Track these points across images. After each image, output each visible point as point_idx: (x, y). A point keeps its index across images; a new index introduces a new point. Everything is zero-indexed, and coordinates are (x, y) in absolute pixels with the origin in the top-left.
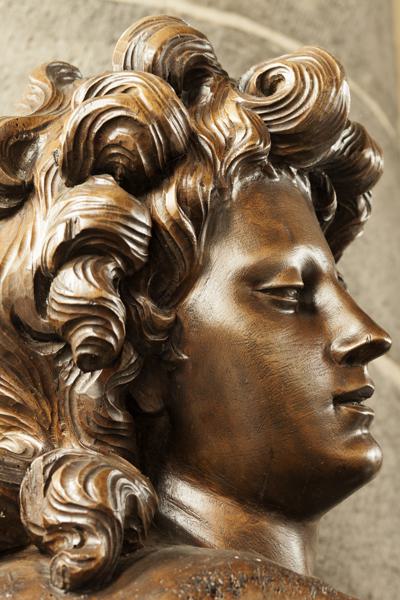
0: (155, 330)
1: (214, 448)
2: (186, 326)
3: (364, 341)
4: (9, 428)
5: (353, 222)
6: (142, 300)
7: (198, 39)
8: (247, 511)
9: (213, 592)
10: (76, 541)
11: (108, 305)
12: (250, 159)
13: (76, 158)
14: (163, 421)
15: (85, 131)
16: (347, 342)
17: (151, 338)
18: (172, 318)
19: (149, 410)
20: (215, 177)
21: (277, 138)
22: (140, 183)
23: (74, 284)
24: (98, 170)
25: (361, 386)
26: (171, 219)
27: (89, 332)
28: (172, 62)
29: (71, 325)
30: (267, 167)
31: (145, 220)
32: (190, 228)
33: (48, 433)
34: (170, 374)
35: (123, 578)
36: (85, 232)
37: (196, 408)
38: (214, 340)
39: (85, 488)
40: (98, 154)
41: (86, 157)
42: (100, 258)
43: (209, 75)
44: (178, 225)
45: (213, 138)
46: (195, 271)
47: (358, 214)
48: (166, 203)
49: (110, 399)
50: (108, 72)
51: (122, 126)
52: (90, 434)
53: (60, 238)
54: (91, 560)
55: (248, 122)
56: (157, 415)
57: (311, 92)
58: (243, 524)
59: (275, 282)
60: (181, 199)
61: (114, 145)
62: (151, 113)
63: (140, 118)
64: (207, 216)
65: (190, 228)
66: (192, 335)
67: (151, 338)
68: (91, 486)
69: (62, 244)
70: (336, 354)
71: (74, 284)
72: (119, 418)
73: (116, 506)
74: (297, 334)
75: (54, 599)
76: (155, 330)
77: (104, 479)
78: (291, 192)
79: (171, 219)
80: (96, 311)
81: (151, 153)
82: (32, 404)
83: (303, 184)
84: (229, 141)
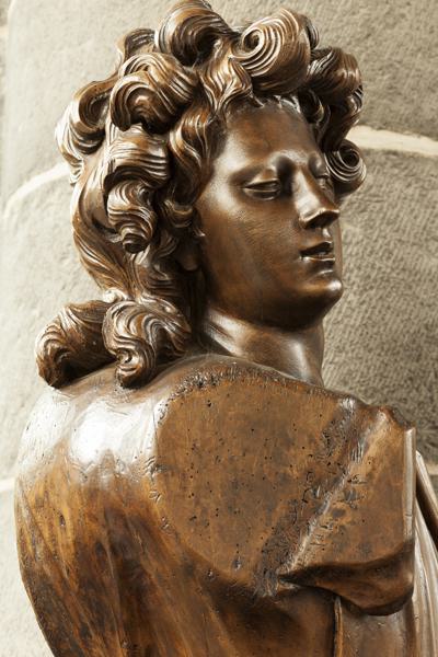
0: (177, 221)
1: (229, 291)
2: (202, 214)
3: (318, 213)
4: (111, 286)
5: (346, 117)
6: (168, 203)
7: (205, 16)
8: (255, 328)
9: (201, 385)
10: (127, 359)
11: (136, 213)
12: (237, 99)
13: (120, 116)
14: (200, 274)
15: (120, 99)
16: (309, 215)
17: (178, 226)
18: (190, 210)
19: (189, 269)
20: (213, 115)
21: (256, 81)
22: (158, 127)
23: (118, 201)
24: (135, 122)
25: (321, 242)
26: (180, 150)
27: (129, 230)
28: (186, 34)
29: (119, 225)
30: (253, 100)
31: (160, 153)
32: (195, 154)
33: (128, 288)
34: (198, 245)
35: (158, 377)
36: (119, 168)
37: (215, 266)
38: (222, 221)
39: (128, 326)
40: (132, 112)
41: (126, 114)
42: (131, 182)
43: (217, 38)
44: (185, 154)
45: (214, 87)
46: (207, 175)
47: (349, 110)
48: (175, 138)
49: (157, 267)
50: (254, 18)
51: (141, 94)
52: (149, 290)
53: (105, 174)
54: (133, 369)
55: (233, 73)
56: (197, 271)
57: (276, 43)
58: (253, 337)
59: (257, 180)
60: (185, 135)
61: (138, 106)
62: (158, 83)
63: (151, 88)
64: (211, 143)
65: (195, 154)
66: (205, 221)
67: (178, 226)
68: (132, 325)
69: (107, 177)
70: (302, 223)
71: (118, 201)
72: (166, 277)
73: (147, 337)
74: (273, 213)
75: (437, 303)
76: (177, 221)
77: (139, 321)
78: (290, 112)
79: (180, 150)
80: (130, 217)
81: (163, 110)
82: (117, 271)
83: (291, 104)
84: (225, 87)
